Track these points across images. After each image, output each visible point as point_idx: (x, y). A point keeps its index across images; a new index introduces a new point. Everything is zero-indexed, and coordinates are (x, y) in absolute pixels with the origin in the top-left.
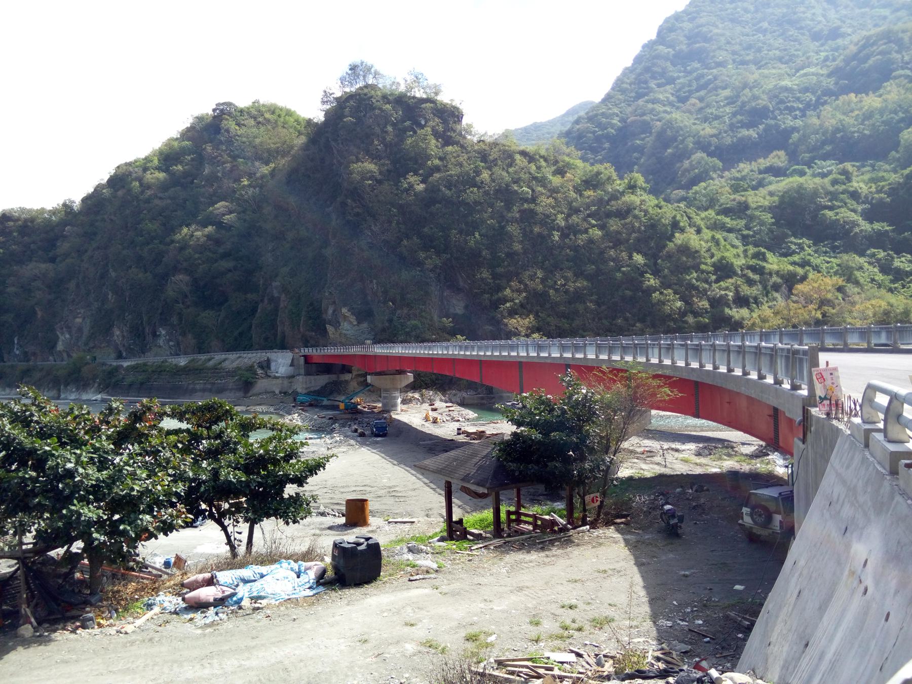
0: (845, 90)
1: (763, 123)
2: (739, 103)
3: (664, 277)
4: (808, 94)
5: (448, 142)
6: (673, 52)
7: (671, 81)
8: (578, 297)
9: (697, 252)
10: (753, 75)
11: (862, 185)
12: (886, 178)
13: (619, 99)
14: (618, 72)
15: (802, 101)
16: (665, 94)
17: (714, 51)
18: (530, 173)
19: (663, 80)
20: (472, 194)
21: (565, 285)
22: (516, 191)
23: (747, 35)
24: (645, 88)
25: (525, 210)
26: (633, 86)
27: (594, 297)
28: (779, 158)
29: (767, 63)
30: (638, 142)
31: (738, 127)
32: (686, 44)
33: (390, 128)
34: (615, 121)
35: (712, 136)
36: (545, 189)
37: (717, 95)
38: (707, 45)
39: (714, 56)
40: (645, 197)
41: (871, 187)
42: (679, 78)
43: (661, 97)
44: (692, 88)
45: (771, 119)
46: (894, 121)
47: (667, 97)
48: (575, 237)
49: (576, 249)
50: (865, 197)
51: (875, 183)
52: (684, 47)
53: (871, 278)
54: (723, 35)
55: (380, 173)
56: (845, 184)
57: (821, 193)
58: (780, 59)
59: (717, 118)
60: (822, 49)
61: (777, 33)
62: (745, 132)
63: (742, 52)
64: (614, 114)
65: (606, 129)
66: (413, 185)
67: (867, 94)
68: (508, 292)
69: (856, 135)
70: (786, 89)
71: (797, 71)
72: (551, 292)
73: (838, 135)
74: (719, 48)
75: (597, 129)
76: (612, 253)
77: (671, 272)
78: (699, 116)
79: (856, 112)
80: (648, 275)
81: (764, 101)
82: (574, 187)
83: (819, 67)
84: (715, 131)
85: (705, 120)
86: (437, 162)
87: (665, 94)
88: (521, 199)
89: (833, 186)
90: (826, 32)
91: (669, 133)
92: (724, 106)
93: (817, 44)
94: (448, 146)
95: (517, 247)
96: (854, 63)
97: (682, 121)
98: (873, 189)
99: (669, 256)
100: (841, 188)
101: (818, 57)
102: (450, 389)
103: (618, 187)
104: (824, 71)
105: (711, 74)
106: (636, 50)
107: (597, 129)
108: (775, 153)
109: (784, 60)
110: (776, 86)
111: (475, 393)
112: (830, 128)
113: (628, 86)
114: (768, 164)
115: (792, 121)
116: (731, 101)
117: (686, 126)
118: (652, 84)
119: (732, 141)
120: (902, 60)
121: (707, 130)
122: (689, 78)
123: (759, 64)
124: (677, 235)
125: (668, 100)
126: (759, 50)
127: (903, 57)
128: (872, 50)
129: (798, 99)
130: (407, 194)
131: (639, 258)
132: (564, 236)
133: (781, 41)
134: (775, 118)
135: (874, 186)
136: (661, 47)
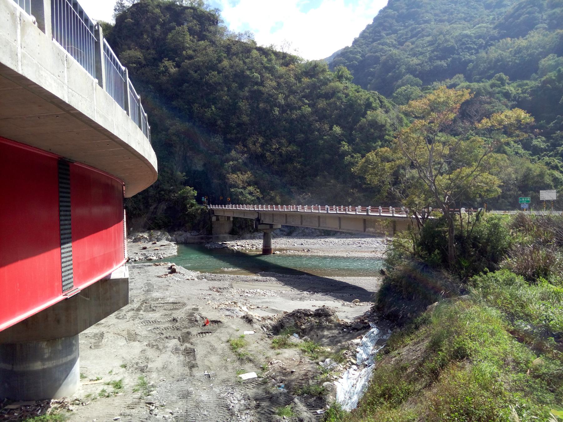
0: (503, 36)
1: (451, 57)
2: (436, 45)
3: (357, 144)
4: (481, 39)
5: (202, 37)
6: (397, 14)
7: (395, 32)
8: (289, 158)
9: (383, 126)
10: (446, 27)
11: (512, 89)
12: (529, 84)
13: (362, 43)
14: (363, 28)
15: (477, 44)
16: (391, 39)
17: (423, 13)
18: (262, 64)
19: (390, 31)
20: (214, 77)
21: (278, 149)
22: (248, 75)
23: (445, 4)
24: (378, 36)
25: (255, 91)
26: (371, 35)
27: (302, 159)
28: (460, 79)
29: (456, 21)
30: (371, 69)
31: (434, 60)
32: (406, 9)
33: (158, 27)
34: (358, 56)
35: (418, 65)
36: (272, 76)
37: (423, 40)
38: (419, 10)
39: (423, 17)
40: (348, 84)
41: (518, 90)
42: (400, 30)
43: (388, 41)
44: (408, 36)
45: (457, 54)
46: (536, 54)
47: (391, 42)
48: (291, 112)
49: (291, 121)
50: (513, 97)
51: (521, 88)
52: (404, 11)
53: (515, 152)
54: (430, 4)
55: (145, 59)
56: (500, 87)
57: (483, 93)
58: (465, 19)
59: (421, 53)
60: (491, 14)
61: (464, 4)
62: (439, 63)
63: (441, 15)
64: (358, 51)
65: (352, 61)
66: (168, 68)
67: (518, 39)
68: (233, 153)
69: (510, 63)
70: (467, 36)
71: (474, 26)
72: (268, 154)
73: (499, 64)
74: (427, 12)
75: (346, 61)
76: (317, 125)
77: (362, 141)
78: (411, 53)
79: (511, 49)
80: (344, 143)
81: (452, 43)
82: (295, 75)
83: (489, 24)
84: (419, 62)
85: (414, 55)
86: (190, 52)
87: (391, 39)
88: (252, 82)
89: (492, 88)
90: (494, 4)
91: (390, 62)
92: (427, 46)
93: (488, 11)
94: (201, 40)
95: (245, 118)
96: (511, 19)
97: (399, 56)
98: (520, 91)
99: (362, 128)
100: (497, 89)
101: (488, 18)
102: (179, 230)
103: (328, 77)
104: (492, 26)
105: (420, 27)
106: (375, 13)
107: (346, 61)
108: (457, 76)
109: (466, 20)
110: (460, 34)
111: (197, 234)
112: (494, 59)
113: (368, 34)
114: (452, 83)
115: (469, 56)
116: (431, 43)
117: (401, 59)
118: (383, 34)
119: (430, 68)
120: (542, 18)
121: (415, 61)
122: (406, 30)
123: (450, 21)
124: (369, 112)
125: (392, 43)
126: (452, 14)
127: (542, 16)
128: (523, 11)
129: (474, 43)
130: (163, 75)
131: (337, 129)
132: (283, 111)
133: (466, 8)
134: (459, 54)
135: (520, 89)
136: (390, 10)
